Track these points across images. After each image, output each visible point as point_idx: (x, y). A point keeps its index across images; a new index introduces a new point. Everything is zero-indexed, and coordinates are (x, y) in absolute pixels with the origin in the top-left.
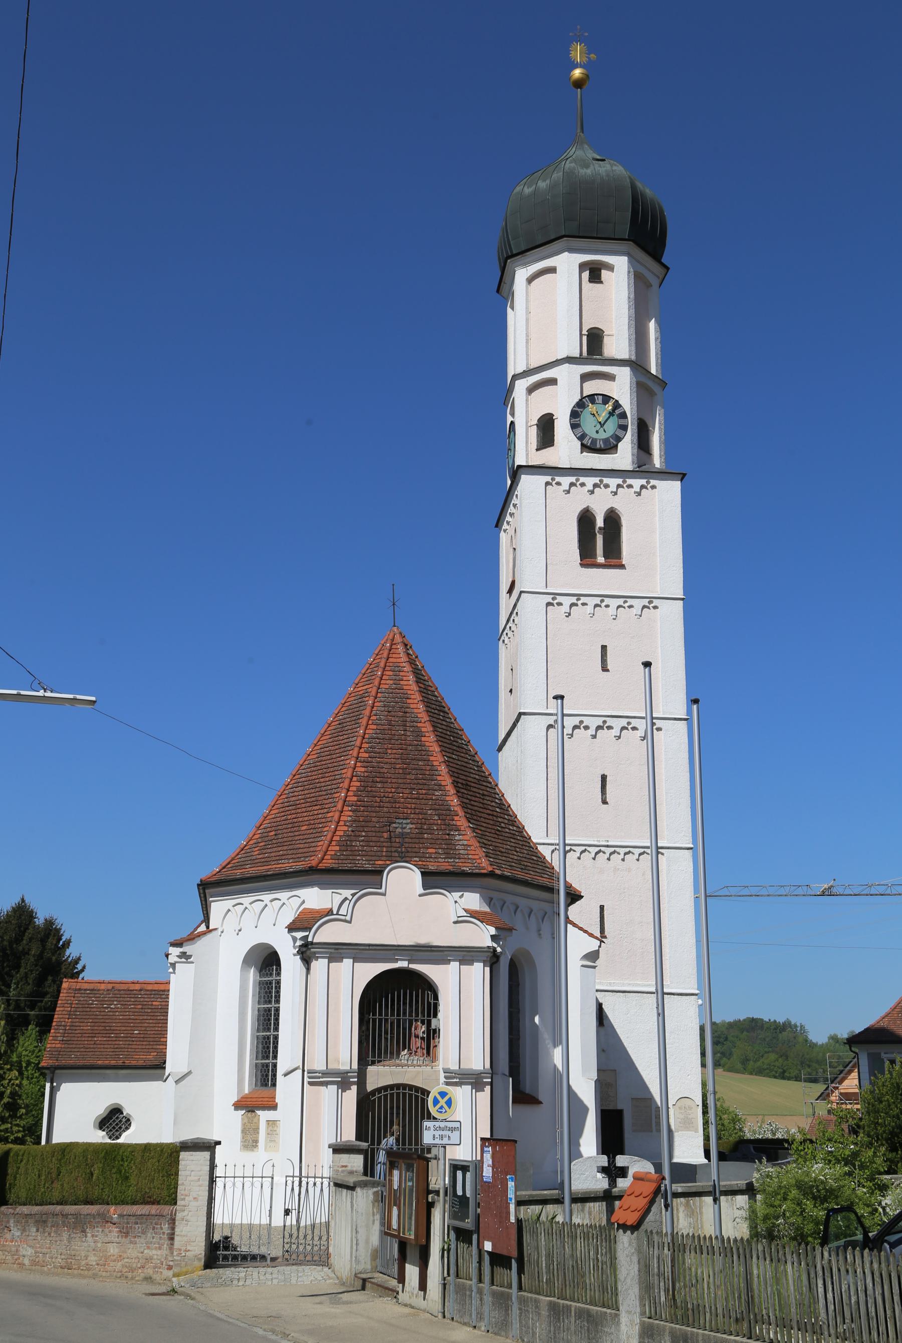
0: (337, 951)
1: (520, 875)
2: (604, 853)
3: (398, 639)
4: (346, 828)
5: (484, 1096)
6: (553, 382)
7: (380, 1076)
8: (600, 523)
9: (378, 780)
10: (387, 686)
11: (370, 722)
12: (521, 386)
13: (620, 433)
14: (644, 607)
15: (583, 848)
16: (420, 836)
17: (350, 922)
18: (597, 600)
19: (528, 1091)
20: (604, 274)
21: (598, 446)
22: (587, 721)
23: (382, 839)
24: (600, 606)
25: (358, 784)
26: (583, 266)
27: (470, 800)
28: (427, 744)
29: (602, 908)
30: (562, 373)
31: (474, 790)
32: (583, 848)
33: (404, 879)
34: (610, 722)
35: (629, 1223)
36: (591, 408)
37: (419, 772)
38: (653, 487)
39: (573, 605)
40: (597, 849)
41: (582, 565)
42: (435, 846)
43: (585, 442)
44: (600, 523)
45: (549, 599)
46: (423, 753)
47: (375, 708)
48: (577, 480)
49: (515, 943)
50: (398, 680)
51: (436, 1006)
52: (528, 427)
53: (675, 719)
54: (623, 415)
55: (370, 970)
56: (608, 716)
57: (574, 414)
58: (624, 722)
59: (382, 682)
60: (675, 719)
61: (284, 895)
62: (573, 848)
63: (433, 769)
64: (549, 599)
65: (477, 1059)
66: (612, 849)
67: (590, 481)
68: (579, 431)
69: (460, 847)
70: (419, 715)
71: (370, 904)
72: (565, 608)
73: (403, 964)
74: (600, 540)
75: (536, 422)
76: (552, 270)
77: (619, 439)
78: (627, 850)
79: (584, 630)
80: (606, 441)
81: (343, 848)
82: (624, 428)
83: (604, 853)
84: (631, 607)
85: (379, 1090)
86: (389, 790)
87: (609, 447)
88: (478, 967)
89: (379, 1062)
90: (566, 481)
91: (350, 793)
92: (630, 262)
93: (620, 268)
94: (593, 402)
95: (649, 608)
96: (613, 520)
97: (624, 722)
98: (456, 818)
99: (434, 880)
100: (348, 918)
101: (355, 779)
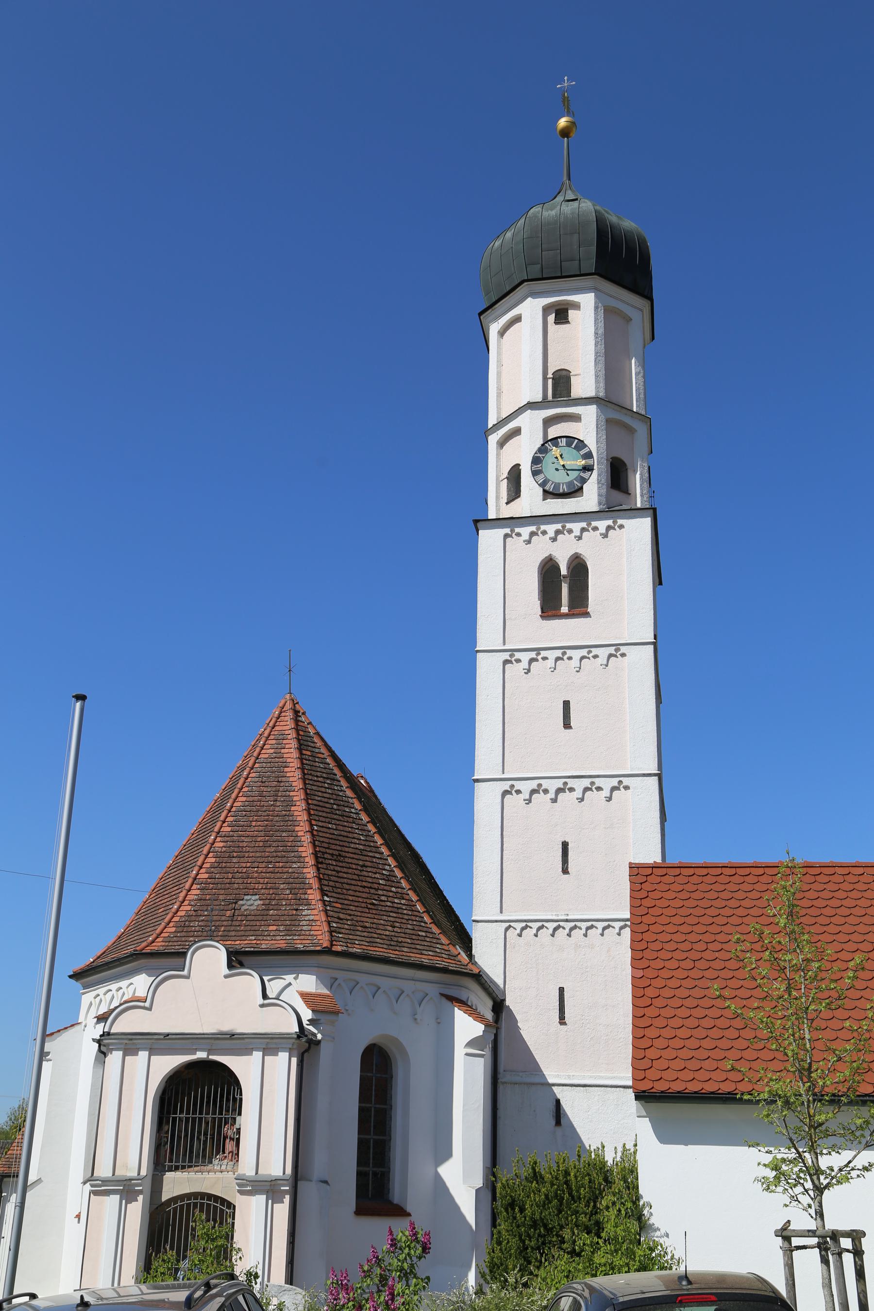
0: (132, 1043)
1: (392, 955)
2: (564, 928)
3: (289, 706)
4: (189, 908)
5: (282, 1210)
6: (517, 432)
7: (178, 1183)
8: (564, 571)
9: (235, 854)
10: (267, 756)
11: (241, 794)
12: (493, 440)
14: (611, 656)
15: (540, 924)
16: (265, 913)
17: (150, 1009)
18: (558, 653)
19: (396, 1199)
20: (571, 313)
21: (561, 491)
22: (545, 784)
23: (223, 918)
24: (562, 659)
25: (213, 860)
26: (546, 310)
27: (338, 872)
28: (296, 813)
29: (561, 990)
31: (350, 861)
32: (540, 924)
33: (210, 958)
34: (571, 783)
36: (555, 451)
37: (280, 844)
38: (621, 527)
39: (532, 661)
40: (555, 924)
42: (276, 923)
43: (547, 488)
44: (564, 571)
45: (506, 656)
46: (289, 821)
47: (249, 780)
48: (538, 529)
50: (279, 747)
52: (498, 482)
53: (644, 775)
54: (589, 455)
55: (167, 1064)
56: (569, 777)
58: (586, 783)
59: (263, 751)
60: (644, 775)
62: (529, 924)
63: (297, 840)
65: (276, 1162)
66: (573, 924)
67: (551, 529)
68: (541, 478)
69: (304, 923)
70: (294, 784)
71: (173, 988)
72: (525, 664)
73: (201, 1055)
74: (563, 589)
75: (506, 475)
77: (584, 481)
78: (589, 924)
79: (545, 686)
80: (570, 484)
81: (180, 929)
83: (564, 928)
84: (596, 657)
85: (174, 1200)
86: (244, 865)
87: (575, 491)
88: (284, 1056)
89: (183, 1167)
90: (525, 531)
91: (203, 871)
92: (596, 296)
93: (586, 305)
94: (557, 445)
95: (616, 656)
97: (586, 783)
98: (309, 891)
99: (237, 960)
100: (147, 1004)
101: (211, 855)
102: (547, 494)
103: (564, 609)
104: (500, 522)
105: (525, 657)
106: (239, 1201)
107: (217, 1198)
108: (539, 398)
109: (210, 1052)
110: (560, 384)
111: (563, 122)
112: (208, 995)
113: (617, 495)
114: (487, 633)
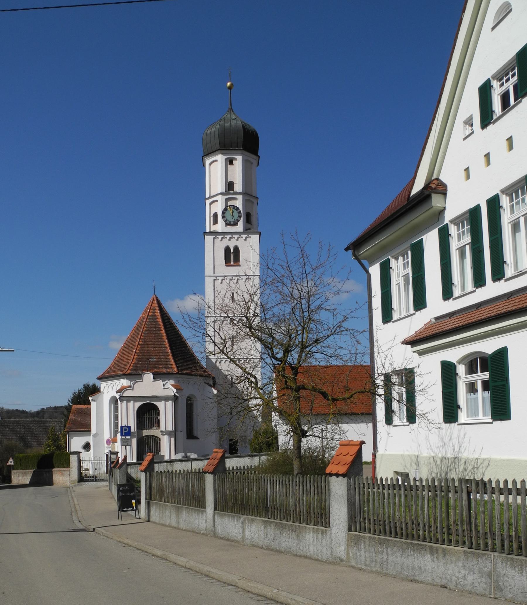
0: (129, 399)
3: (155, 299)
6: (216, 201)
7: (145, 433)
8: (232, 251)
12: (208, 202)
13: (239, 219)
17: (133, 390)
19: (195, 435)
20: (234, 161)
26: (226, 159)
30: (219, 198)
33: (148, 377)
35: (340, 473)
39: (223, 280)
41: (226, 266)
44: (232, 251)
49: (187, 393)
50: (154, 312)
51: (159, 413)
52: (210, 217)
54: (240, 212)
55: (138, 404)
57: (223, 213)
61: (114, 382)
64: (215, 278)
68: (238, 211)
72: (220, 281)
74: (232, 256)
76: (216, 161)
77: (238, 221)
80: (234, 222)
82: (240, 217)
85: (145, 436)
87: (235, 224)
96: (236, 249)
99: (156, 377)
102: (227, 225)
103: (232, 263)
104: (211, 233)
105: (220, 278)
106: (161, 437)
107: (154, 436)
108: (224, 191)
109: (150, 401)
110: (230, 186)
111: (229, 84)
112: (149, 386)
113: (249, 226)
114: (209, 270)
